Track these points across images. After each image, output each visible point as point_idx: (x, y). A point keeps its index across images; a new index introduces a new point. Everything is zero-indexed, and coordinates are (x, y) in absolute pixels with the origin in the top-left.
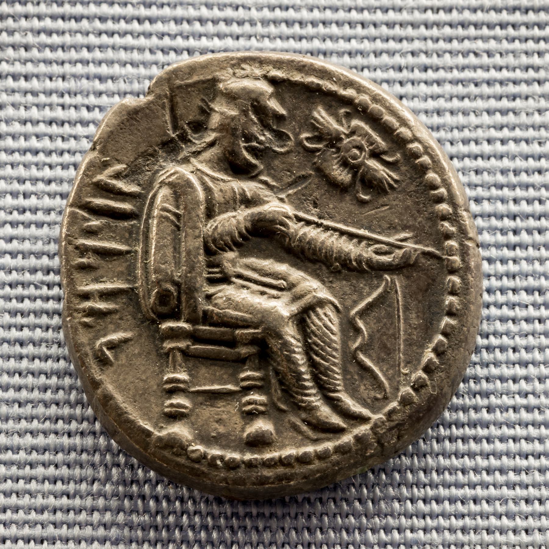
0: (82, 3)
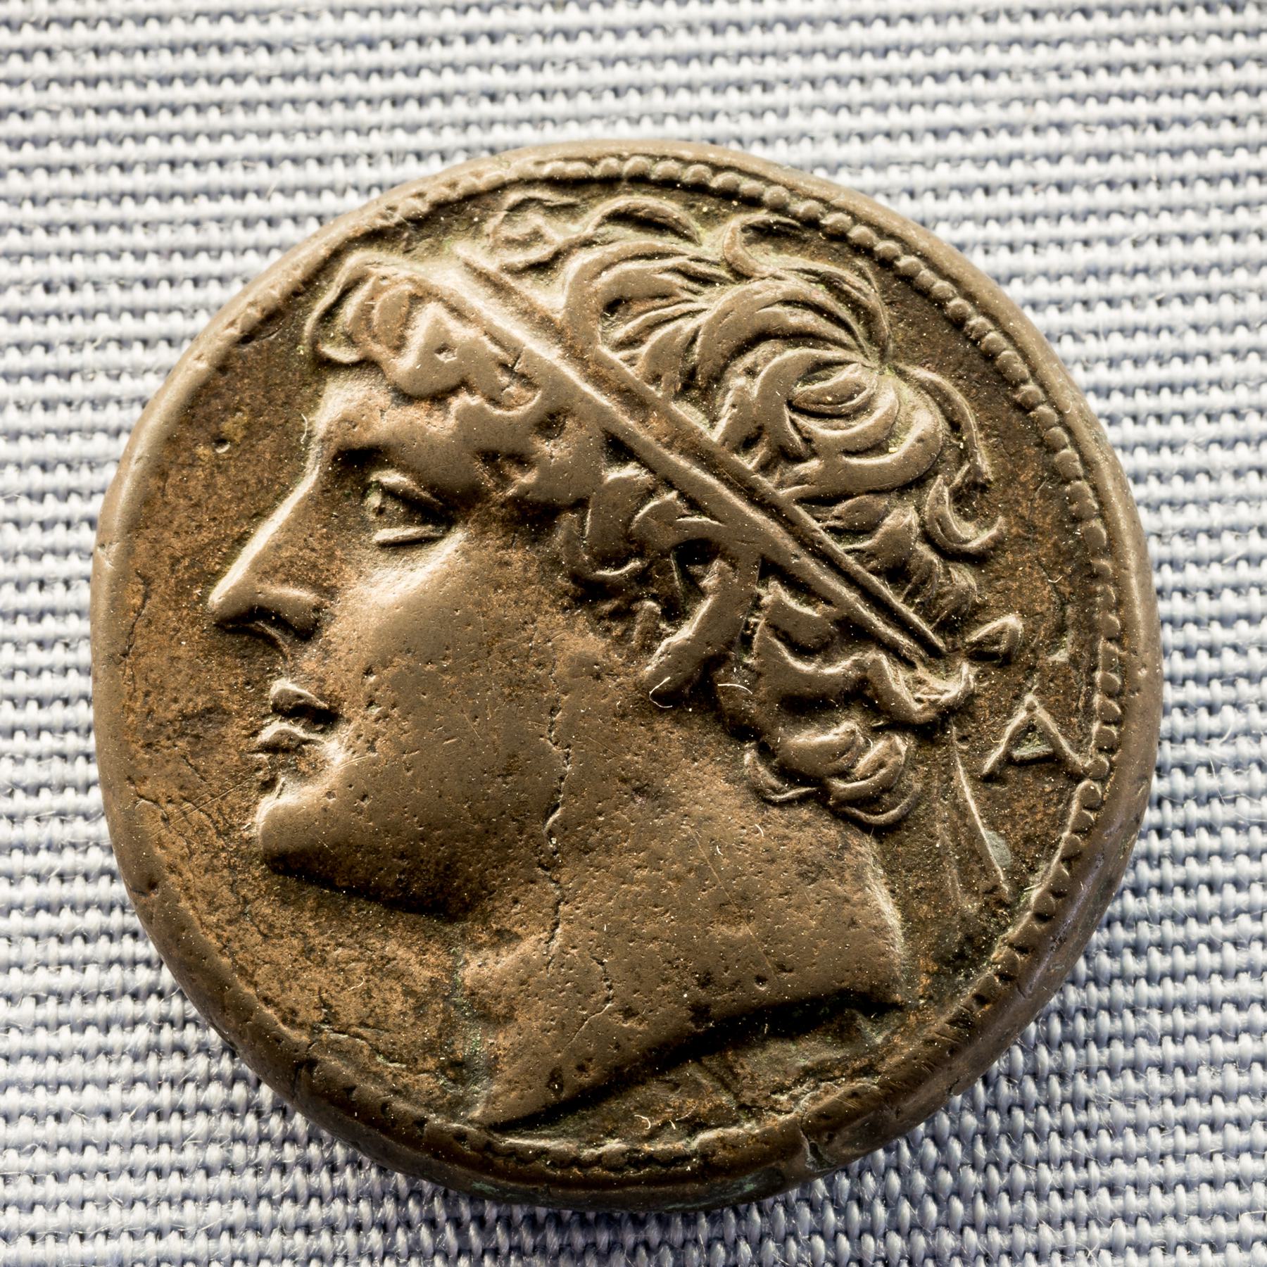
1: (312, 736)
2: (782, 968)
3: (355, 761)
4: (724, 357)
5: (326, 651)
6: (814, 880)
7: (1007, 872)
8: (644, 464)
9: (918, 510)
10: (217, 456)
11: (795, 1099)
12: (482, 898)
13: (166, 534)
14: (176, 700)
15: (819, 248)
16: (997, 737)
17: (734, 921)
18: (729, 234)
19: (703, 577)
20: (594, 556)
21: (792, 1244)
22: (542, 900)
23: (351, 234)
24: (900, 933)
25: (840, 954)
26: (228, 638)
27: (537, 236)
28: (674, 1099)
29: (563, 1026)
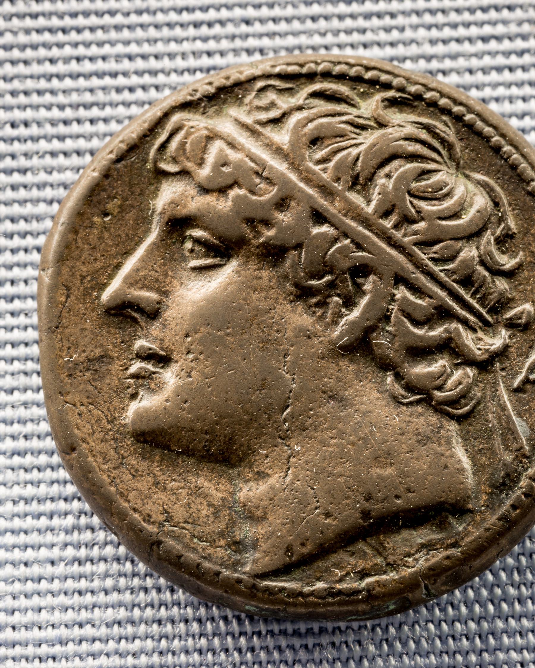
0: (319, 3)
1: (157, 370)
2: (409, 491)
3: (181, 383)
4: (374, 168)
5: (164, 325)
6: (425, 444)
7: (527, 440)
8: (332, 225)
9: (478, 248)
10: (104, 222)
11: (416, 560)
12: (249, 455)
13: (78, 264)
14: (84, 351)
15: (423, 110)
16: (521, 368)
17: (383, 466)
18: (375, 103)
19: (364, 285)
20: (307, 274)
21: (417, 627)
22: (281, 456)
23: (174, 104)
24: (470, 472)
25: (439, 483)
26: (112, 318)
27: (273, 105)
28: (352, 560)
29: (293, 522)
